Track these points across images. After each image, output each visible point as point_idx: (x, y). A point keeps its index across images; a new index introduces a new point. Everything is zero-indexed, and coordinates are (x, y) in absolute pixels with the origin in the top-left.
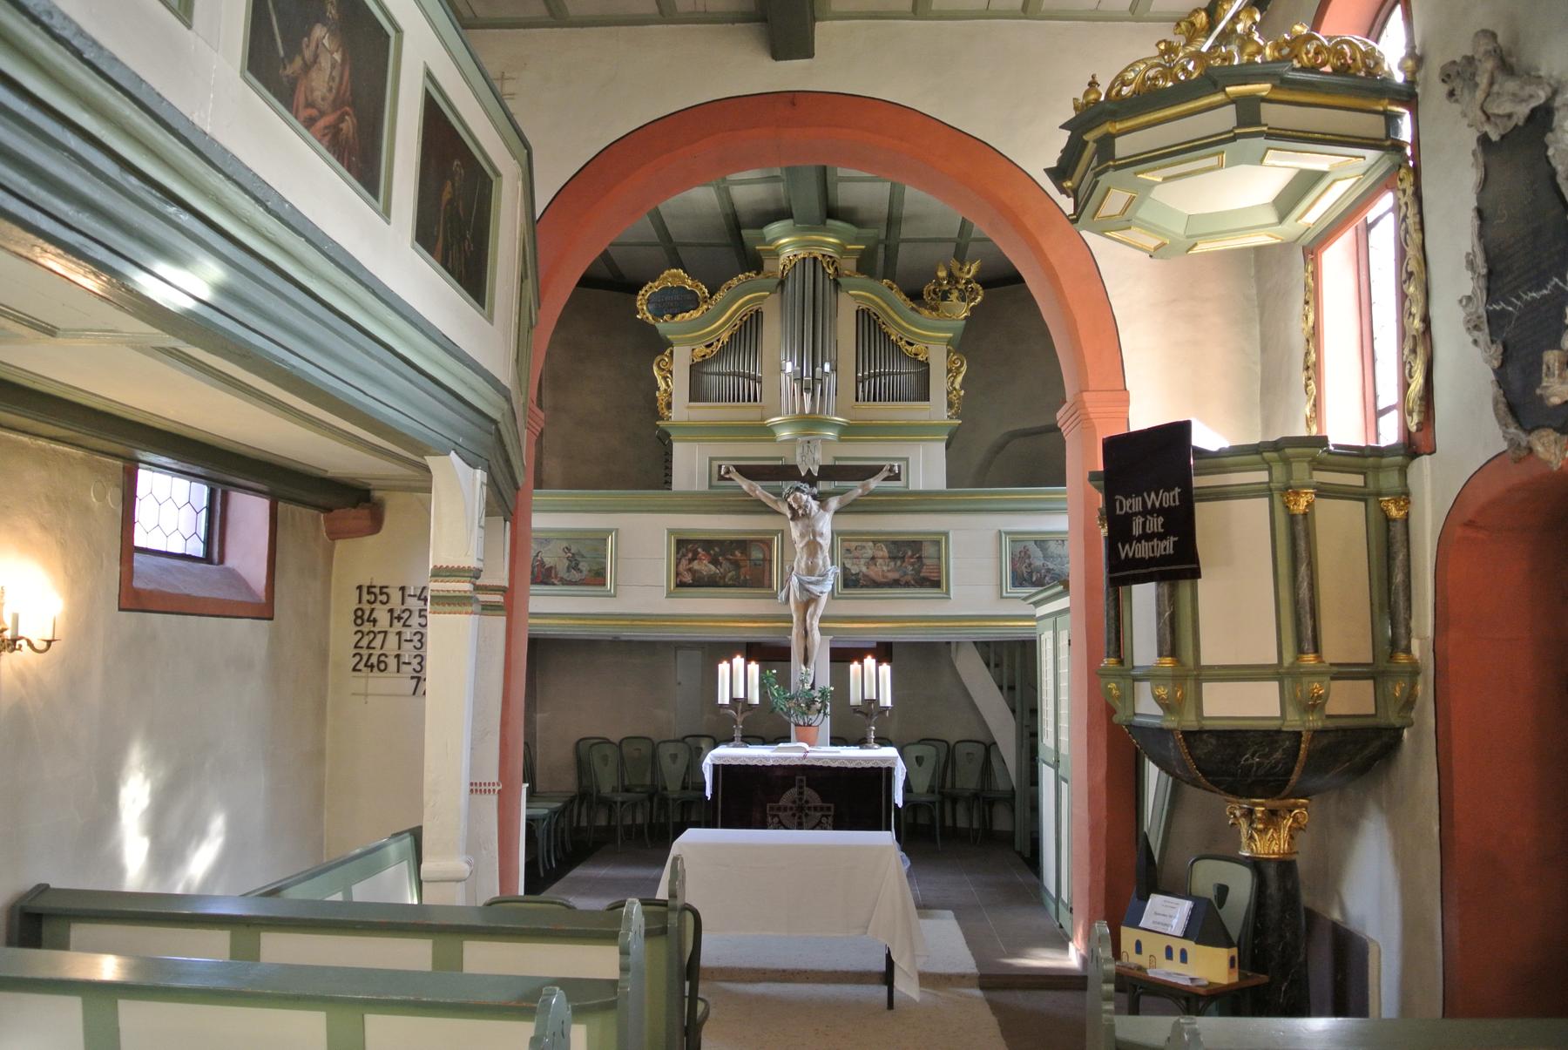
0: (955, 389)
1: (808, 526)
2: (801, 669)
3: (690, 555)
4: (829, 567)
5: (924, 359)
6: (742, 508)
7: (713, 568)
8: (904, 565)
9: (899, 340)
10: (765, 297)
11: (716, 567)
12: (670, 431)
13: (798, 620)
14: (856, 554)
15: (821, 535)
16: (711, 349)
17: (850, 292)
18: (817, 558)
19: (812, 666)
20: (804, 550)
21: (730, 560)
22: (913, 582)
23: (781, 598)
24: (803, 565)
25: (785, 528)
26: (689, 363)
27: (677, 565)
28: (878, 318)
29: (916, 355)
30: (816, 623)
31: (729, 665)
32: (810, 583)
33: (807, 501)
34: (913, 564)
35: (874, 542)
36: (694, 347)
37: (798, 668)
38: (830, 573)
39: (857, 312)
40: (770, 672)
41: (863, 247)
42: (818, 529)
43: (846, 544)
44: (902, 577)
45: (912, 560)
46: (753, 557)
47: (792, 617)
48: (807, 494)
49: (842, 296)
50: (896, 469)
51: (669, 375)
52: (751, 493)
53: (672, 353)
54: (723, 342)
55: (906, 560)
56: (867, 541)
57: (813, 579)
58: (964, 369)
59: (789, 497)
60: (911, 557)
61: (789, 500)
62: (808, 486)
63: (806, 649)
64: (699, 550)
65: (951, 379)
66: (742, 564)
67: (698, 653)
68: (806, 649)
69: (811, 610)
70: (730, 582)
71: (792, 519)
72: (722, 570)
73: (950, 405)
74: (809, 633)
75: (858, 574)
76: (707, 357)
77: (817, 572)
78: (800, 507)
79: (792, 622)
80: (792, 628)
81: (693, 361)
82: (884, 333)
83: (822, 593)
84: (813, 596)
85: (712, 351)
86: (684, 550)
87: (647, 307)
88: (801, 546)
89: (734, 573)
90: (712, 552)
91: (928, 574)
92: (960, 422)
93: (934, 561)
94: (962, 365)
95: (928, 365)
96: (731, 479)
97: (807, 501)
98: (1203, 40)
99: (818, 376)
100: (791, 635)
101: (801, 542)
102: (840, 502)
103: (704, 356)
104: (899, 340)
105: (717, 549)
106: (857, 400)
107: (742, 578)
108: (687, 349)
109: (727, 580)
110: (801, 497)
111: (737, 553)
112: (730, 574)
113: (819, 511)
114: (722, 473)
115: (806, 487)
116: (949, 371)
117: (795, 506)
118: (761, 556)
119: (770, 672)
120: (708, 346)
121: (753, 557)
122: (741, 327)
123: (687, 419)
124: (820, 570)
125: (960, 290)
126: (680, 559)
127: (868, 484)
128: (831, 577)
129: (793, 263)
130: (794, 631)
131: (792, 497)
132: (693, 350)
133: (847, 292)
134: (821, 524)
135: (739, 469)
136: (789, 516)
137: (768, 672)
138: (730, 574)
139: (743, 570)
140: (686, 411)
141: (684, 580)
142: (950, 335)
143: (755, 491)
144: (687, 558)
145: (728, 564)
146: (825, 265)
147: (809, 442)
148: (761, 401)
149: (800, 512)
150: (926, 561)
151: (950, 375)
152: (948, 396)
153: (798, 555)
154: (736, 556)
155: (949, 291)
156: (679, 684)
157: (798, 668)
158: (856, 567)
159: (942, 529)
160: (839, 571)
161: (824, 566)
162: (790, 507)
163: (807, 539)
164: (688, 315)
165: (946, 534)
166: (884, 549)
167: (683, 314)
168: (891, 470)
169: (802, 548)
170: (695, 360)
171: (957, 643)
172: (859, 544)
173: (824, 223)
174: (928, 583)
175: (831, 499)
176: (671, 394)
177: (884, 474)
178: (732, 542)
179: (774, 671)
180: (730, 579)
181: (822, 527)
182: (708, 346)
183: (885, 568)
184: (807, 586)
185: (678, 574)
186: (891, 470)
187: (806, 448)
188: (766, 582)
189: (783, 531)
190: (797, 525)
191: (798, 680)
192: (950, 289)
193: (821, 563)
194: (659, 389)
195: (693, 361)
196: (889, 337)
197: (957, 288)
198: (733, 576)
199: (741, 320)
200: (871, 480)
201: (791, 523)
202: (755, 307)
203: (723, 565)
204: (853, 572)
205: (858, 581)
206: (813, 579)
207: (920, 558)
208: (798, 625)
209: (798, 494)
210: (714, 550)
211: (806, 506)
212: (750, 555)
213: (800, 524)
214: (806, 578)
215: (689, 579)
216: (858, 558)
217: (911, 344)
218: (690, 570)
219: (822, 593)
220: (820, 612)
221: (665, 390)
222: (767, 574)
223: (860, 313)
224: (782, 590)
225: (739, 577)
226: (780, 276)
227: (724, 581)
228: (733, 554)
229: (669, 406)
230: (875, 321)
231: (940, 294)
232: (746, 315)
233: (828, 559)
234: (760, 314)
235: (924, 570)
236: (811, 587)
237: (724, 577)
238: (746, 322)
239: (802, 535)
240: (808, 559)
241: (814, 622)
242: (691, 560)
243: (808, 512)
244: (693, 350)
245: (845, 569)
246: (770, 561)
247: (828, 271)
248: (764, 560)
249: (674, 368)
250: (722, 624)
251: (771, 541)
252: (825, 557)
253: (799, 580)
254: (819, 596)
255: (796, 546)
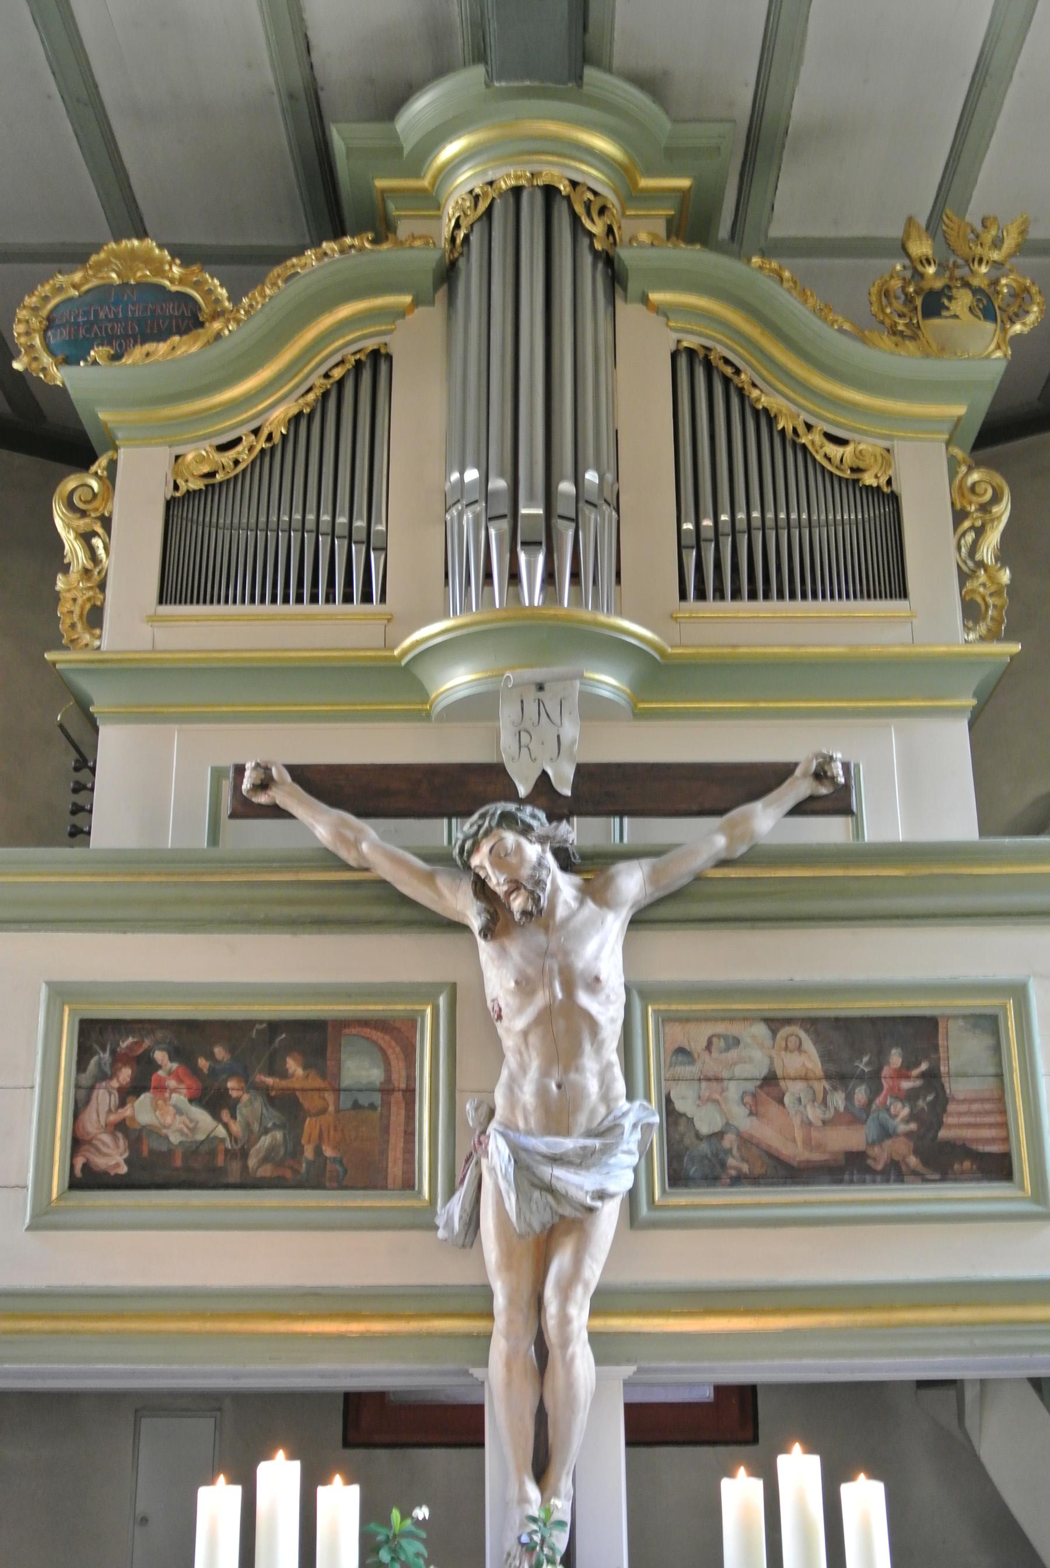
0: (981, 564)
1: (545, 954)
2: (524, 1500)
3: (126, 1074)
4: (623, 1104)
5: (883, 481)
6: (316, 911)
7: (203, 1117)
8: (878, 1101)
9: (801, 429)
10: (400, 313)
11: (216, 1116)
12: (87, 686)
13: (511, 1301)
14: (709, 1064)
15: (594, 984)
16: (232, 454)
17: (655, 297)
18: (579, 1069)
19: (565, 1485)
20: (533, 1039)
21: (265, 1091)
22: (913, 1161)
23: (449, 1224)
24: (528, 1094)
25: (460, 975)
26: (162, 492)
27: (78, 1112)
28: (738, 372)
29: (855, 470)
30: (580, 1315)
31: (236, 1491)
32: (557, 1160)
33: (540, 864)
34: (910, 1097)
35: (774, 1023)
36: (178, 450)
37: (513, 1492)
38: (627, 1123)
39: (674, 356)
40: (406, 1514)
41: (685, 183)
42: (580, 964)
43: (678, 1035)
44: (872, 1144)
45: (906, 1085)
46: (346, 1081)
47: (487, 1293)
48: (542, 840)
49: (628, 312)
50: (838, 770)
51: (99, 530)
52: (344, 854)
53: (112, 465)
54: (270, 438)
55: (886, 1084)
56: (747, 1018)
57: (568, 1144)
58: (1003, 510)
59: (476, 847)
60: (902, 1073)
61: (475, 861)
62: (542, 815)
63: (541, 1417)
64: (160, 1056)
65: (970, 537)
66: (309, 1102)
67: (205, 1426)
68: (541, 1417)
69: (559, 1264)
70: (266, 1171)
71: (488, 932)
72: (236, 1127)
73: (971, 611)
74: (555, 1353)
75: (719, 1135)
76: (219, 477)
77: (582, 1120)
78: (516, 886)
79: (490, 1315)
80: (488, 1336)
81: (176, 487)
82: (756, 413)
83: (602, 1195)
84: (568, 1211)
85: (236, 462)
86: (106, 1056)
87: (45, 338)
88: (520, 1023)
89: (279, 1135)
90: (203, 1063)
91: (968, 1133)
92: (1016, 648)
93: (985, 1087)
94: (996, 499)
95: (894, 499)
96: (276, 812)
97: (540, 864)
98: (391, 1395)
99: (565, 507)
100: (485, 1363)
101: (521, 1010)
102: (653, 878)
103: (212, 475)
104: (801, 429)
105: (219, 1052)
106: (683, 596)
107: (309, 1153)
108: (162, 455)
109: (252, 1162)
110: (519, 848)
111: (293, 1065)
112: (265, 1141)
113: (582, 902)
114: (246, 785)
115: (535, 817)
116: (959, 516)
117: (497, 882)
118: (375, 1075)
119: (406, 1514)
120: (223, 448)
121: (346, 1081)
122: (325, 395)
123: (149, 647)
124: (593, 1112)
125: (976, 291)
126: (92, 1088)
127: (747, 818)
128: (631, 1140)
129: (483, 206)
130: (498, 1348)
131: (485, 848)
132: (177, 457)
133: (645, 300)
134: (590, 948)
135: (302, 776)
136: (476, 923)
137: (396, 1514)
138: (265, 1141)
139: (310, 1126)
140: (146, 629)
141: (101, 1162)
142: (959, 410)
143: (356, 844)
144: (115, 1084)
145: (258, 1104)
146: (579, 209)
147: (541, 687)
148: (383, 599)
149: (517, 904)
150: (956, 1088)
151: (967, 524)
152: (962, 585)
153: (511, 1060)
154: (284, 1074)
155: (946, 292)
156: (144, 1520)
157: (513, 1492)
158: (710, 1109)
159: (1003, 973)
160: (656, 1119)
161: (606, 1096)
162: (481, 888)
163: (540, 999)
164: (162, 347)
165: (1019, 992)
166: (808, 1044)
167: (149, 347)
168: (820, 775)
169: (525, 1034)
170: (183, 487)
171: (983, 1382)
172: (720, 1028)
173: (579, 78)
174: (967, 1164)
175: (622, 867)
176: (102, 586)
177: (799, 788)
178: (274, 1027)
179: (422, 1513)
180: (265, 1160)
181: (597, 958)
182: (223, 448)
183: (814, 1113)
184: (548, 1172)
185: (77, 1143)
186: (820, 775)
187: (531, 708)
188: (395, 1170)
189: (453, 987)
190: (503, 953)
191: (510, 1544)
192: (949, 287)
193: (593, 1086)
194: (66, 569)
195: (176, 487)
196: (771, 420)
197: (966, 285)
198: (272, 1149)
199: (327, 376)
200: (758, 806)
201: (485, 949)
202: (370, 344)
203: (242, 1110)
204: (704, 1129)
205: (723, 1165)
206: (568, 1144)
207: (933, 1078)
208: (510, 1322)
209: (510, 838)
210: (210, 1056)
211: (539, 883)
212: (338, 1075)
213: (515, 948)
214: (542, 1144)
215: (120, 1159)
216: (718, 1079)
217: (841, 442)
218: (121, 1127)
219: (602, 1195)
220: (593, 1272)
221: (86, 572)
222: (396, 1141)
223: (683, 362)
224: (451, 1192)
225: (296, 1151)
226: (444, 245)
227: (245, 1167)
228: (275, 1069)
229: (95, 618)
230: (726, 381)
231: (919, 302)
232: (342, 362)
233: (618, 1072)
234: (383, 367)
235: (948, 1120)
236: (565, 1177)
237: (244, 1154)
238: (340, 383)
239: (525, 987)
240: (545, 1073)
241: (573, 1311)
242: (129, 1093)
243: (544, 902)
244: (177, 457)
245: (671, 1113)
246: (410, 1094)
247: (588, 225)
248: (386, 1090)
249: (117, 509)
250: (233, 1326)
251: (412, 1022)
252: (609, 1066)
253: (517, 1152)
254: (591, 1210)
255: (501, 1028)
